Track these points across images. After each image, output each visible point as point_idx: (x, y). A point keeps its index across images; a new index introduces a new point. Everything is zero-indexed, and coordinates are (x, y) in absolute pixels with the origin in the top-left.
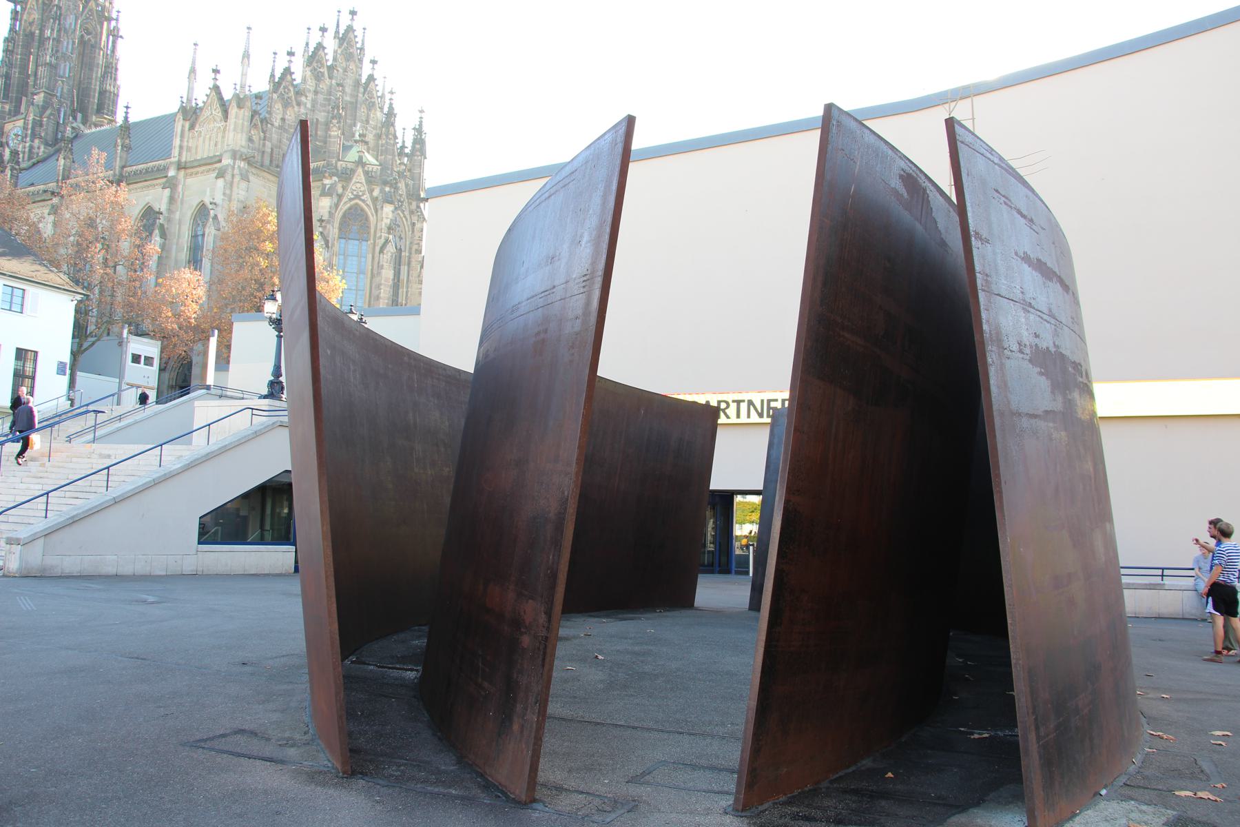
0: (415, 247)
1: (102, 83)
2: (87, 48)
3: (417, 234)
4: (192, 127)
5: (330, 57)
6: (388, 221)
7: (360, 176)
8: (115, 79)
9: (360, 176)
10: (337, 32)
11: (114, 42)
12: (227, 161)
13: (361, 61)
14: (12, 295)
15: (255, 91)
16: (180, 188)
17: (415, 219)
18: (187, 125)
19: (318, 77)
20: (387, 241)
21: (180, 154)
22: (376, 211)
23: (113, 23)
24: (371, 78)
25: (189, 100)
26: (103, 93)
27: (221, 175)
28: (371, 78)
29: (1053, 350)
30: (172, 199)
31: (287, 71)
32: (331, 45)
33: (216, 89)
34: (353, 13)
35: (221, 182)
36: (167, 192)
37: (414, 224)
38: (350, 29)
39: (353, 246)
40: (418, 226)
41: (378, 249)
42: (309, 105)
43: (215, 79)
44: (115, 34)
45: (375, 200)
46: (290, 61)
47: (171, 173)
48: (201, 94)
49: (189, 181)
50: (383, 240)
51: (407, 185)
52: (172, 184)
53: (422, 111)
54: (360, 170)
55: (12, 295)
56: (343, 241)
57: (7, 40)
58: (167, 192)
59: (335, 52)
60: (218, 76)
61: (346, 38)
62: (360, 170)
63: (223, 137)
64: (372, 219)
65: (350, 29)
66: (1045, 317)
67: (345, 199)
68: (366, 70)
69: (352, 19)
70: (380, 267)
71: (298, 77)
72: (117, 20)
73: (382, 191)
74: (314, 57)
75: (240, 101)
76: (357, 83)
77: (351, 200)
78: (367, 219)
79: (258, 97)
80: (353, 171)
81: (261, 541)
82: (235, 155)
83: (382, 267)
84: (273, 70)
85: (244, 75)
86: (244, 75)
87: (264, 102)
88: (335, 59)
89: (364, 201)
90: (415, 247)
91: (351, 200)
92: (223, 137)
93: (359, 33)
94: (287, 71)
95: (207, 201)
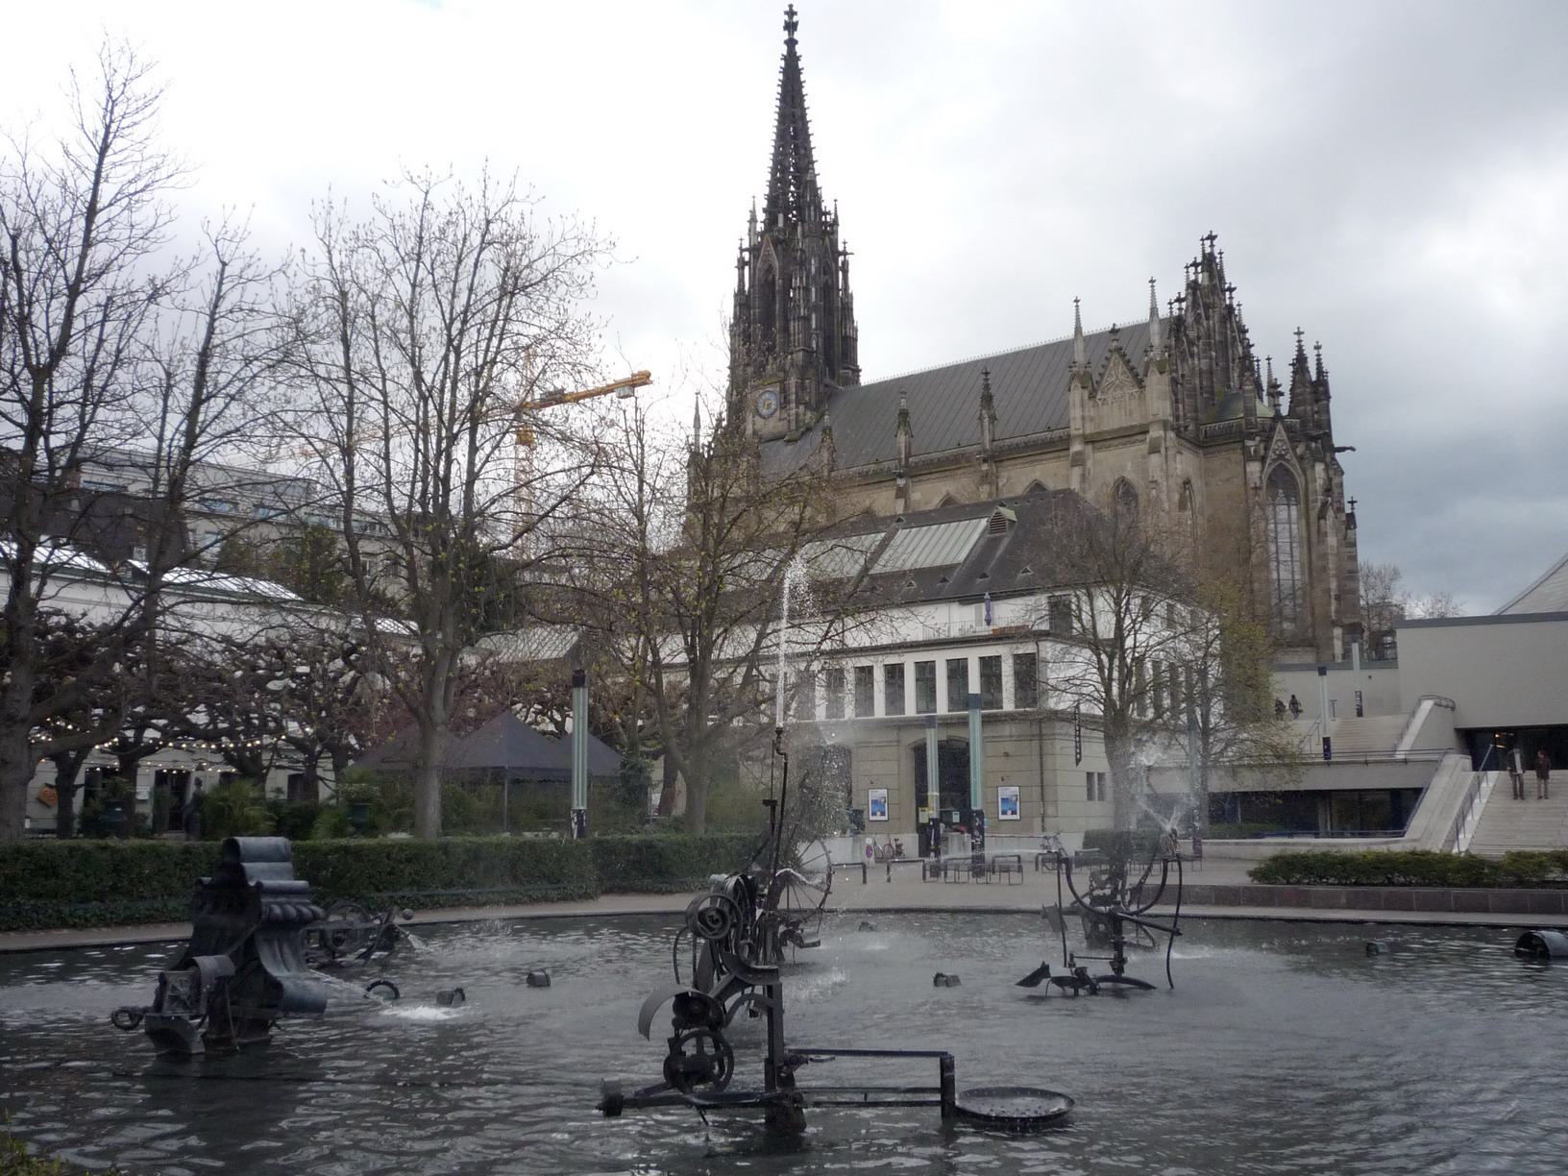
4: (1092, 396)
7: (1280, 433)
9: (1280, 433)
12: (1156, 432)
16: (1089, 464)
18: (1086, 393)
22: (1304, 471)
27: (1154, 449)
29: (789, 900)
35: (1155, 459)
38: (1211, 254)
40: (1336, 480)
41: (1314, 515)
45: (1301, 458)
49: (1100, 455)
52: (1078, 460)
53: (1299, 333)
54: (1279, 426)
62: (1279, 426)
64: (1300, 480)
66: (1366, 1084)
70: (1322, 535)
73: (1308, 447)
80: (1272, 429)
82: (1165, 425)
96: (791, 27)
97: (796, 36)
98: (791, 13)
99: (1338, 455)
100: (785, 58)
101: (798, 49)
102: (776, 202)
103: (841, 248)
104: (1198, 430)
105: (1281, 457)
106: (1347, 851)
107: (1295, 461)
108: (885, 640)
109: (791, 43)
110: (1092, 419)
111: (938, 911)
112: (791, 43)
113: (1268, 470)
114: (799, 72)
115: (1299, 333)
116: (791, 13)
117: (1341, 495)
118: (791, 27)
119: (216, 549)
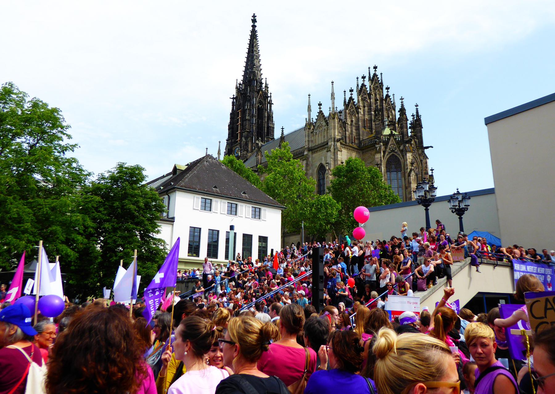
0: (424, 172)
1: (268, 124)
2: (261, 111)
3: (424, 165)
5: (368, 89)
6: (410, 160)
8: (272, 121)
10: (370, 77)
11: (270, 107)
13: (382, 89)
14: (205, 203)
15: (339, 110)
16: (310, 159)
17: (422, 158)
19: (363, 100)
20: (411, 170)
21: (308, 144)
22: (403, 156)
23: (269, 98)
24: (388, 96)
25: (309, 119)
26: (268, 127)
28: (388, 96)
30: (307, 165)
31: (351, 99)
32: (367, 83)
33: (321, 113)
34: (375, 68)
36: (305, 162)
37: (421, 161)
38: (375, 75)
39: (394, 175)
40: (424, 161)
41: (407, 175)
42: (362, 113)
43: (320, 108)
44: (271, 103)
46: (352, 94)
47: (306, 153)
48: (314, 116)
49: (314, 155)
50: (409, 170)
51: (415, 142)
52: (306, 158)
55: (205, 203)
56: (389, 173)
57: (231, 114)
58: (305, 162)
59: (370, 87)
60: (321, 107)
61: (374, 79)
62: (392, 138)
63: (327, 133)
65: (375, 75)
67: (387, 153)
68: (385, 93)
69: (375, 71)
70: (410, 183)
71: (356, 100)
72: (271, 97)
74: (361, 90)
75: (333, 115)
76: (382, 100)
77: (390, 153)
78: (399, 160)
79: (340, 112)
80: (389, 139)
81: (259, 247)
83: (410, 184)
84: (345, 99)
85: (333, 103)
86: (333, 103)
87: (343, 114)
88: (370, 89)
89: (396, 152)
90: (424, 172)
91: (390, 153)
92: (327, 133)
93: (379, 76)
94: (351, 99)
95: (324, 162)
96: (254, 21)
97: (256, 24)
98: (254, 16)
99: (426, 151)
101: (256, 29)
103: (269, 95)
105: (393, 151)
106: (492, 357)
107: (399, 153)
109: (254, 26)
110: (312, 141)
112: (254, 26)
113: (387, 157)
116: (254, 16)
117: (426, 167)
118: (254, 21)
119: (251, 340)
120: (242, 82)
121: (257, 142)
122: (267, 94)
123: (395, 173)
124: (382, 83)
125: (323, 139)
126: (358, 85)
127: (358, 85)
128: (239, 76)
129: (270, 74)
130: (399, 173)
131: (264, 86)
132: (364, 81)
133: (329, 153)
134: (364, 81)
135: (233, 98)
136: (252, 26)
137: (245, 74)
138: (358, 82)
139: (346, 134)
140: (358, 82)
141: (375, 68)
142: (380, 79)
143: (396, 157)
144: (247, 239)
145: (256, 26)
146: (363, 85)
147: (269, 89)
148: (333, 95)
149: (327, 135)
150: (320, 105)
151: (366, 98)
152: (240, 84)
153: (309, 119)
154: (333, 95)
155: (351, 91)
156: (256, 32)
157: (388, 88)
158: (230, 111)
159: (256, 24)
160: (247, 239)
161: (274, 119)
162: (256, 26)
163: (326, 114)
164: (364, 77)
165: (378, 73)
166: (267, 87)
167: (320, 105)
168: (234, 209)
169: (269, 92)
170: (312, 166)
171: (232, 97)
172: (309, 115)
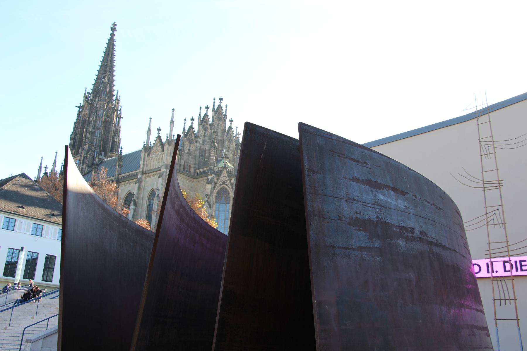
4: (149, 155)
5: (211, 120)
7: (225, 173)
8: (119, 136)
9: (225, 173)
10: (214, 108)
11: (119, 120)
13: (225, 121)
18: (146, 154)
21: (143, 168)
23: (119, 112)
24: (230, 128)
26: (113, 143)
28: (230, 128)
30: (139, 188)
32: (210, 114)
33: (159, 138)
34: (221, 99)
38: (220, 107)
47: (139, 176)
49: (147, 179)
52: (139, 182)
54: (225, 171)
56: (217, 204)
57: (75, 123)
59: (213, 117)
61: (218, 112)
62: (225, 171)
63: (162, 159)
65: (220, 107)
67: (218, 185)
68: (228, 125)
69: (221, 102)
71: (196, 130)
72: (120, 110)
74: (203, 121)
77: (221, 185)
88: (213, 121)
89: (227, 185)
91: (221, 185)
92: (162, 159)
93: (224, 108)
94: (191, 128)
95: (155, 188)
96: (113, 29)
97: (115, 33)
98: (114, 25)
100: (109, 40)
101: (115, 38)
102: (96, 91)
103: (119, 109)
104: (195, 172)
105: (224, 183)
107: (229, 185)
108: (17, 255)
109: (112, 35)
111: (488, 235)
112: (112, 35)
114: (114, 45)
115: (151, 119)
116: (114, 25)
118: (113, 29)
120: (91, 92)
121: (101, 157)
122: (117, 107)
123: (224, 205)
124: (226, 115)
125: (157, 164)
126: (200, 115)
127: (200, 115)
128: (89, 85)
129: (122, 85)
130: (227, 205)
131: (114, 98)
132: (207, 111)
133: (161, 179)
134: (207, 111)
135: (80, 107)
136: (111, 34)
137: (96, 82)
138: (200, 112)
139: (180, 162)
140: (200, 112)
141: (221, 99)
142: (224, 111)
143: (226, 189)
144: (516, 262)
145: (115, 35)
146: (206, 115)
147: (120, 102)
148: (172, 122)
149: (162, 161)
150: (159, 130)
151: (207, 128)
152: (89, 93)
153: (171, 136)
154: (172, 122)
155: (192, 120)
156: (114, 41)
157: (231, 121)
158: (75, 120)
159: (115, 33)
160: (516, 262)
161: (122, 134)
162: (115, 35)
163: (164, 140)
164: (207, 108)
165: (223, 105)
166: (117, 100)
167: (159, 130)
168: (39, 230)
169: (120, 105)
170: (144, 190)
171: (79, 105)
172: (171, 130)
